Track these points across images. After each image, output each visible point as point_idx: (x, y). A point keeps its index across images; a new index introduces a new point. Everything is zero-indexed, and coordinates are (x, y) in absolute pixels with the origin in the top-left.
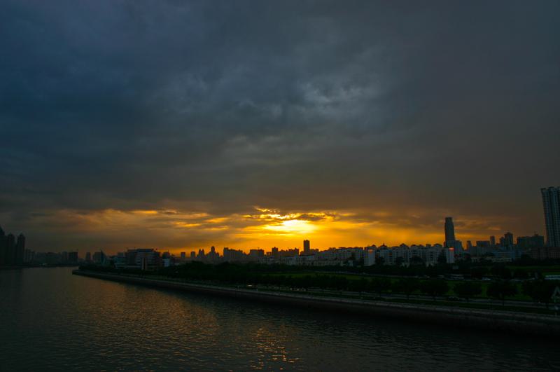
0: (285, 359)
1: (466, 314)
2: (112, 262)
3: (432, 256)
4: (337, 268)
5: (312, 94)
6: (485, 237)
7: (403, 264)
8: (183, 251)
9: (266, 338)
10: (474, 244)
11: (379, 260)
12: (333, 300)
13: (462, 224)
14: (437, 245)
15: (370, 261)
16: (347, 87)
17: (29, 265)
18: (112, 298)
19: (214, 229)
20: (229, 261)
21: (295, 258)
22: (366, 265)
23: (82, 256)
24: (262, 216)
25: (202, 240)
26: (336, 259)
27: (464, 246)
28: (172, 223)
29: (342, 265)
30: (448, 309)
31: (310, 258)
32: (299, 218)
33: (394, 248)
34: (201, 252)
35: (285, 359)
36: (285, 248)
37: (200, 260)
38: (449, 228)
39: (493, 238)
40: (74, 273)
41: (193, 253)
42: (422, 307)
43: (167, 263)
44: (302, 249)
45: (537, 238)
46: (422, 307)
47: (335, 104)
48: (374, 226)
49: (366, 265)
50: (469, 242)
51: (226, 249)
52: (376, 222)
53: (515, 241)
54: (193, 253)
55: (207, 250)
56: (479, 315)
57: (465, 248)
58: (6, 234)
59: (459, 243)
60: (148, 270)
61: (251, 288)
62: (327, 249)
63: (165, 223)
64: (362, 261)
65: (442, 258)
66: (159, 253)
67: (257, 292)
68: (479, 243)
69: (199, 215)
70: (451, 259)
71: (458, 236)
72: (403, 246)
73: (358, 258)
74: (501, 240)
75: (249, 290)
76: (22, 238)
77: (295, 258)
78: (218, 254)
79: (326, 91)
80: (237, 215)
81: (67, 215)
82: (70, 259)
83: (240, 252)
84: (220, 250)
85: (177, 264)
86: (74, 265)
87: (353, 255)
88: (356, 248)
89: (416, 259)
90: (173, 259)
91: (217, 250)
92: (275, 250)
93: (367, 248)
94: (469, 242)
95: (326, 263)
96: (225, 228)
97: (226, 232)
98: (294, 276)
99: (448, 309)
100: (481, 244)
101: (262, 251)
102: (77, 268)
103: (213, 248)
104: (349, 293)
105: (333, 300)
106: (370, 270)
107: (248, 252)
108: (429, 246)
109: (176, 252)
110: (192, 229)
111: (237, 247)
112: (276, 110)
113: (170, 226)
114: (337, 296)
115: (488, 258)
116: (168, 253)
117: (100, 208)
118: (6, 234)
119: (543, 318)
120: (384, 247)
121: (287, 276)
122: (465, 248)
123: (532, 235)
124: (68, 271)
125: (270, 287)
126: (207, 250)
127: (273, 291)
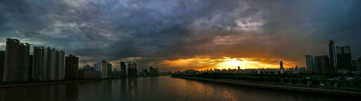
0: (233, 100)
1: (286, 87)
2: (182, 74)
3: (276, 72)
4: (248, 74)
5: (240, 24)
6: (291, 67)
7: (268, 74)
8: (202, 70)
9: (227, 93)
10: (288, 69)
11: (261, 72)
12: (247, 83)
13: (285, 63)
14: (278, 69)
15: (259, 73)
16: (250, 22)
17: (159, 75)
18: (182, 83)
19: (211, 63)
20: (216, 72)
21: (235, 71)
22: (257, 74)
23: (172, 72)
24: (225, 59)
25: (208, 66)
26: (248, 72)
27: (285, 69)
28: (198, 62)
29: (249, 74)
30: (281, 86)
31: (240, 71)
32: (237, 60)
33: (266, 69)
34: (208, 70)
35: (233, 100)
36: (233, 69)
37: (207, 72)
38: (281, 64)
39: (293, 67)
40: (171, 77)
41: (205, 70)
42: (274, 85)
43: (197, 73)
44: (237, 69)
45: (304, 68)
46: (274, 85)
47: (247, 27)
48: (260, 63)
49: (257, 74)
50: (287, 68)
51: (215, 69)
52: (261, 62)
53: (299, 68)
54: (205, 70)
55: (209, 69)
56: (289, 88)
57: (286, 70)
58: (153, 68)
59: (284, 68)
60: (191, 75)
61: (222, 80)
62: (245, 69)
63: (196, 62)
64: (256, 73)
65: (279, 72)
66: (195, 71)
67: (224, 81)
68: (289, 68)
69: (206, 59)
70: (282, 73)
71: (284, 66)
72: (268, 68)
73: (255, 72)
74: (295, 68)
75: (222, 80)
76: (157, 68)
77: (235, 71)
78: (213, 70)
79: (244, 23)
80: (218, 59)
81: (167, 62)
82: (169, 74)
83: (219, 70)
84: (213, 69)
85: (200, 73)
86: (171, 75)
87: (254, 71)
88: (255, 69)
89: (272, 72)
90: (199, 72)
91: (212, 69)
92: (229, 69)
93: (258, 69)
94: (287, 68)
95: (245, 73)
96: (215, 63)
97: (215, 64)
98: (235, 76)
99: (281, 86)
100: (290, 69)
101: (226, 69)
102: (171, 76)
103: (211, 69)
104: (252, 82)
105: (247, 83)
106: (259, 75)
107: (221, 70)
108: (276, 69)
109: (200, 70)
110: (203, 63)
111: (218, 68)
112: (229, 28)
113: (197, 63)
114: (248, 82)
115: (292, 73)
116: (198, 71)
117: (177, 59)
118: (153, 68)
119: (305, 88)
120: (263, 69)
121: (233, 76)
122: (286, 70)
123: (303, 67)
124: (169, 76)
125: (228, 80)
126: (209, 69)
127: (229, 81)
